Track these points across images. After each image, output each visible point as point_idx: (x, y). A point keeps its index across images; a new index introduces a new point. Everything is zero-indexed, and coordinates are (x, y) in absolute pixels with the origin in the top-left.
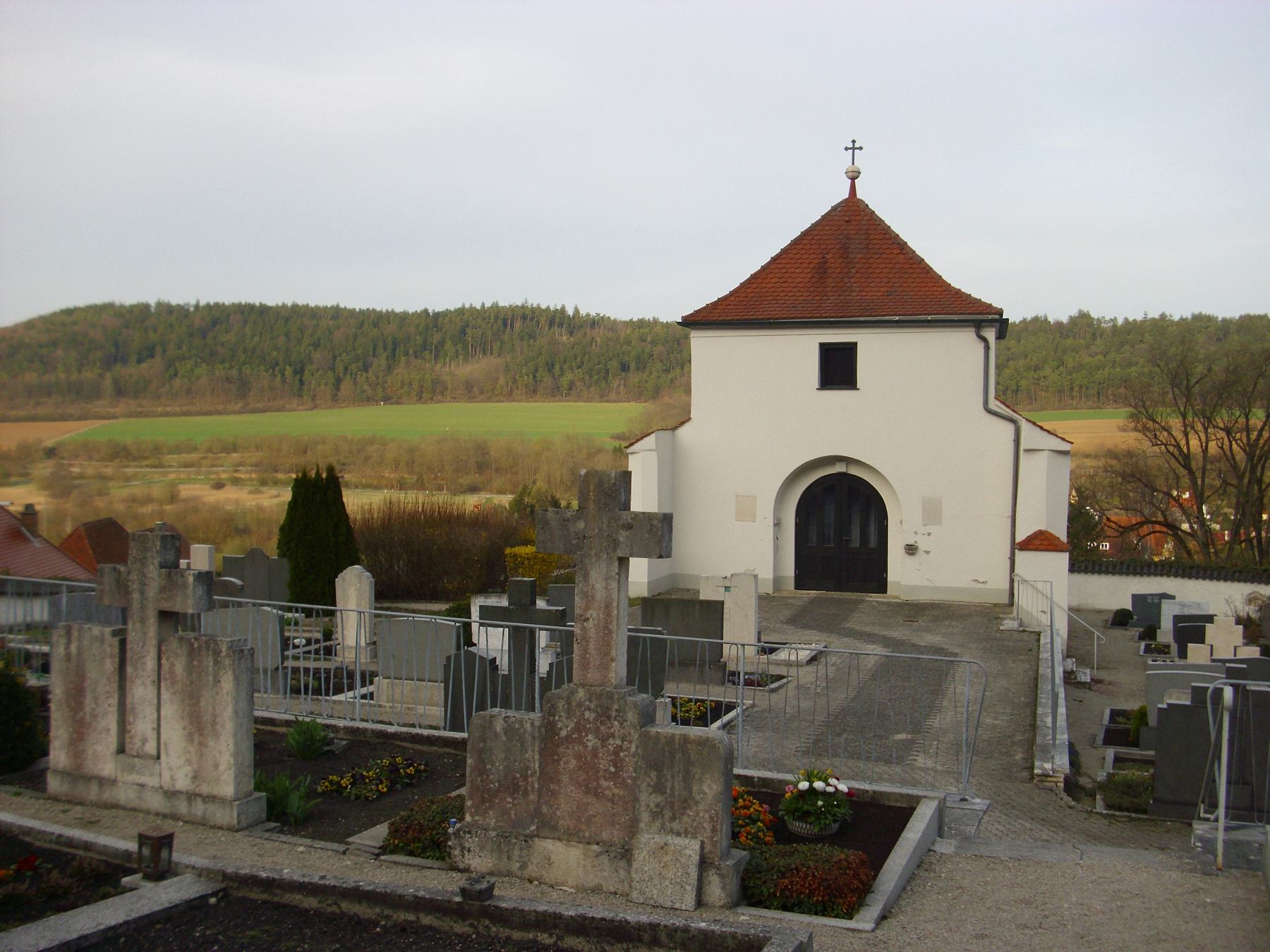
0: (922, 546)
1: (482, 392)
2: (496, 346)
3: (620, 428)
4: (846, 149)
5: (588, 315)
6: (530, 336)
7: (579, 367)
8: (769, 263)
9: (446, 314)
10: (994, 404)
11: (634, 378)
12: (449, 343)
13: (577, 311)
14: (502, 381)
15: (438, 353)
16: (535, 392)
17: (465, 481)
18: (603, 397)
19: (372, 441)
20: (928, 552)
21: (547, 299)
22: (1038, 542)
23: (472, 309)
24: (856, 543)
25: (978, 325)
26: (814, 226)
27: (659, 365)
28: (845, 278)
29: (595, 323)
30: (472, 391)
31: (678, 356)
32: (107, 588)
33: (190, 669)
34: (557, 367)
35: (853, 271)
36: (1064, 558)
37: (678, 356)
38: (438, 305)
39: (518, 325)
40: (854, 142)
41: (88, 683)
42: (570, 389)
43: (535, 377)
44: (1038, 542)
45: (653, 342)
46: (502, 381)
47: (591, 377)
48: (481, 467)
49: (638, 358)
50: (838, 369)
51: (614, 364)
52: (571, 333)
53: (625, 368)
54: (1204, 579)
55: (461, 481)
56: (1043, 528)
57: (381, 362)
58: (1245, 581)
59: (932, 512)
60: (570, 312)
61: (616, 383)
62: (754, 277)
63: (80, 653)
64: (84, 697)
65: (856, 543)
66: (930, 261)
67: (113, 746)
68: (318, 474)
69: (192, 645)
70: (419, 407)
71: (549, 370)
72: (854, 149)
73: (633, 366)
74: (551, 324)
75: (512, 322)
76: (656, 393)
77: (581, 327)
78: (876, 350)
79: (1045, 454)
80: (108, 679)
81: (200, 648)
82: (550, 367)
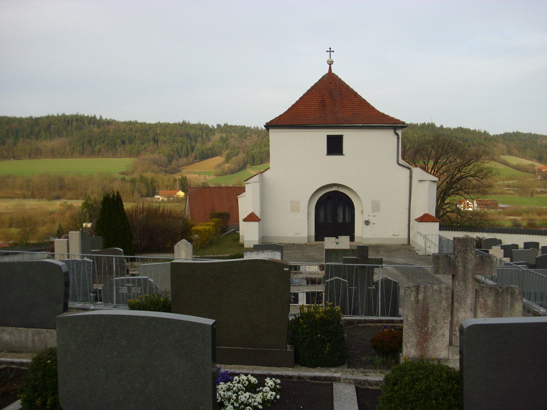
0: (372, 221)
1: (59, 154)
2: (65, 133)
3: (123, 169)
4: (327, 51)
5: (106, 119)
6: (80, 129)
7: (103, 142)
8: (299, 100)
9: (41, 118)
10: (401, 161)
11: (128, 147)
12: (43, 132)
13: (101, 117)
14: (68, 149)
15: (37, 136)
16: (83, 154)
17: (54, 194)
18: (114, 156)
19: (9, 177)
20: (374, 224)
21: (87, 111)
22: (426, 218)
23: (53, 116)
24: (341, 220)
25: (395, 128)
26: (316, 85)
27: (139, 141)
28: (331, 107)
29: (109, 123)
30: (54, 153)
31: (147, 137)
32: (442, 266)
33: (496, 302)
34: (93, 142)
35: (337, 104)
36: (437, 225)
37: (147, 137)
38: (37, 114)
39: (74, 124)
40: (330, 48)
41: (430, 314)
42: (99, 152)
43: (83, 147)
44: (426, 218)
45: (136, 131)
46: (68, 149)
47: (109, 147)
48: (62, 187)
49: (129, 138)
50: (335, 146)
51: (119, 141)
52: (99, 127)
53: (123, 143)
54: (446, 230)
55: (52, 194)
56: (427, 213)
57: (10, 141)
58: (462, 231)
59: (376, 207)
60: (98, 118)
61: (120, 149)
62: (294, 106)
63: (425, 298)
64: (428, 321)
65: (341, 220)
66: (368, 100)
67: (447, 343)
68: (114, 195)
69: (498, 290)
70: (29, 160)
71: (89, 144)
72: (330, 51)
73: (127, 142)
74: (89, 124)
75: (72, 122)
76: (138, 154)
77: (103, 124)
78: (351, 138)
79: (428, 182)
80: (444, 310)
81: (502, 292)
82: (90, 142)
